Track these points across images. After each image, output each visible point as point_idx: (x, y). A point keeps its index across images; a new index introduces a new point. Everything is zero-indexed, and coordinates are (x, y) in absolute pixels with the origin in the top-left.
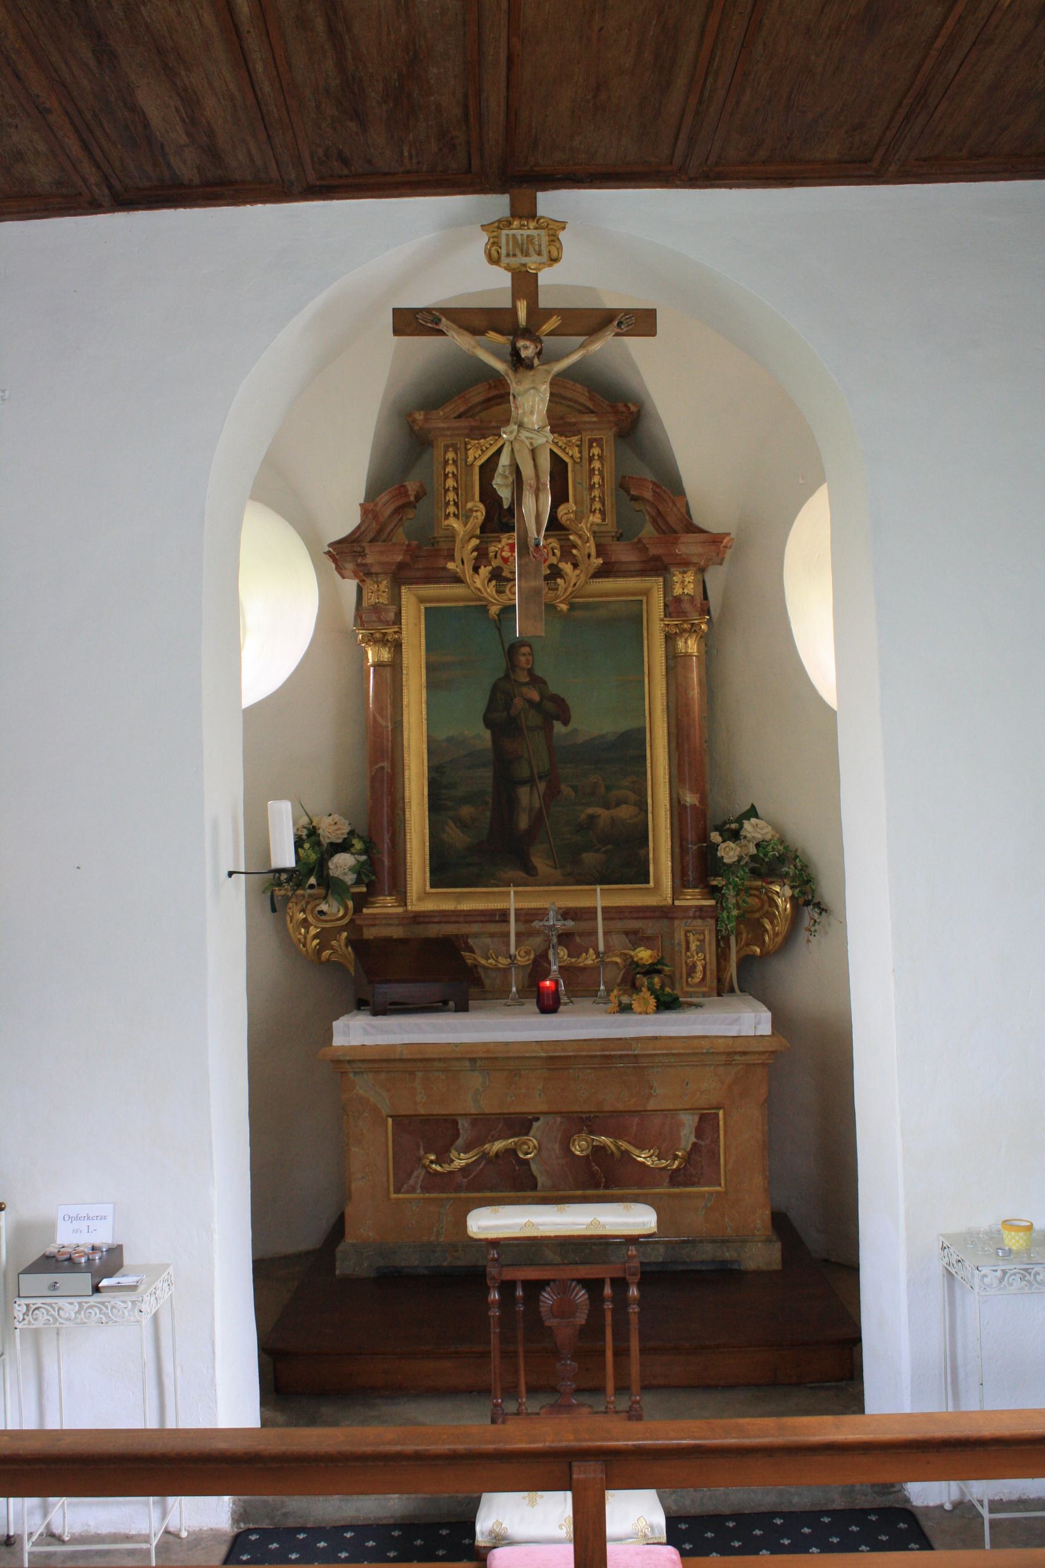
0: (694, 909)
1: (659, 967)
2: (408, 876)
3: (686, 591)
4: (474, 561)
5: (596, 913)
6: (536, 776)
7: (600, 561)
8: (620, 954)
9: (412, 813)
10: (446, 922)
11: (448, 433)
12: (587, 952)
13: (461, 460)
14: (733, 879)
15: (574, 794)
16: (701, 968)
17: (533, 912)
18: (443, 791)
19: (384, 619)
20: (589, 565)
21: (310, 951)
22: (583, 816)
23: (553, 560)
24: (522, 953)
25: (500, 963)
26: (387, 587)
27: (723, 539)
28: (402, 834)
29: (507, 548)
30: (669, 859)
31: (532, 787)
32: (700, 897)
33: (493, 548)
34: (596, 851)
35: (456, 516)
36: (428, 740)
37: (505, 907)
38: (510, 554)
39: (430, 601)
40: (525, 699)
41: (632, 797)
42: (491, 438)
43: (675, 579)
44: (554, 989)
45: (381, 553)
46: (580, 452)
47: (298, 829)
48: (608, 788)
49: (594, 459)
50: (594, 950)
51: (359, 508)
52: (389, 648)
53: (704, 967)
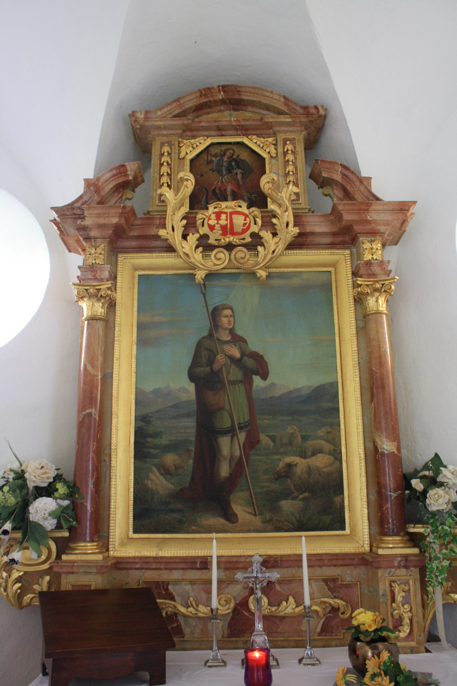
0: (399, 559)
1: (384, 634)
2: (111, 522)
3: (375, 257)
4: (183, 228)
5: (301, 561)
6: (237, 426)
7: (297, 230)
8: (321, 603)
9: (118, 461)
10: (147, 569)
11: (165, 132)
12: (287, 601)
13: (175, 153)
14: (442, 528)
15: (272, 444)
16: (408, 621)
17: (234, 559)
18: (149, 440)
19: (99, 277)
20: (287, 233)
21: (10, 595)
22: (281, 465)
23: (254, 229)
24: (223, 602)
25: (200, 612)
26: (104, 250)
27: (409, 207)
28: (108, 480)
29: (213, 216)
30: (366, 506)
31: (232, 437)
32: (401, 545)
33: (200, 215)
34: (293, 499)
35: (169, 186)
36: (136, 391)
37: (206, 554)
38: (216, 222)
39: (143, 269)
40: (226, 355)
41: (327, 446)
42: (201, 138)
43: (365, 246)
44: (264, 662)
45: (99, 216)
46: (276, 149)
47: (5, 472)
48: (305, 438)
49: (288, 153)
50: (293, 598)
51: (83, 183)
52: (103, 304)
53: (411, 620)
